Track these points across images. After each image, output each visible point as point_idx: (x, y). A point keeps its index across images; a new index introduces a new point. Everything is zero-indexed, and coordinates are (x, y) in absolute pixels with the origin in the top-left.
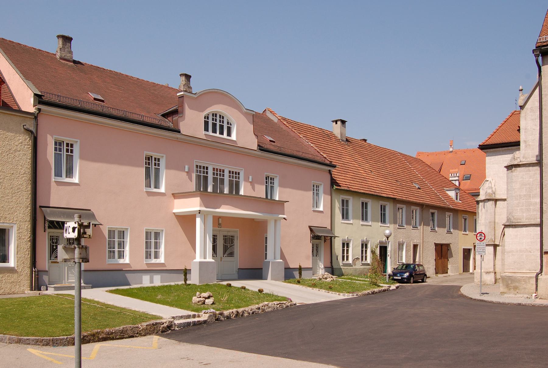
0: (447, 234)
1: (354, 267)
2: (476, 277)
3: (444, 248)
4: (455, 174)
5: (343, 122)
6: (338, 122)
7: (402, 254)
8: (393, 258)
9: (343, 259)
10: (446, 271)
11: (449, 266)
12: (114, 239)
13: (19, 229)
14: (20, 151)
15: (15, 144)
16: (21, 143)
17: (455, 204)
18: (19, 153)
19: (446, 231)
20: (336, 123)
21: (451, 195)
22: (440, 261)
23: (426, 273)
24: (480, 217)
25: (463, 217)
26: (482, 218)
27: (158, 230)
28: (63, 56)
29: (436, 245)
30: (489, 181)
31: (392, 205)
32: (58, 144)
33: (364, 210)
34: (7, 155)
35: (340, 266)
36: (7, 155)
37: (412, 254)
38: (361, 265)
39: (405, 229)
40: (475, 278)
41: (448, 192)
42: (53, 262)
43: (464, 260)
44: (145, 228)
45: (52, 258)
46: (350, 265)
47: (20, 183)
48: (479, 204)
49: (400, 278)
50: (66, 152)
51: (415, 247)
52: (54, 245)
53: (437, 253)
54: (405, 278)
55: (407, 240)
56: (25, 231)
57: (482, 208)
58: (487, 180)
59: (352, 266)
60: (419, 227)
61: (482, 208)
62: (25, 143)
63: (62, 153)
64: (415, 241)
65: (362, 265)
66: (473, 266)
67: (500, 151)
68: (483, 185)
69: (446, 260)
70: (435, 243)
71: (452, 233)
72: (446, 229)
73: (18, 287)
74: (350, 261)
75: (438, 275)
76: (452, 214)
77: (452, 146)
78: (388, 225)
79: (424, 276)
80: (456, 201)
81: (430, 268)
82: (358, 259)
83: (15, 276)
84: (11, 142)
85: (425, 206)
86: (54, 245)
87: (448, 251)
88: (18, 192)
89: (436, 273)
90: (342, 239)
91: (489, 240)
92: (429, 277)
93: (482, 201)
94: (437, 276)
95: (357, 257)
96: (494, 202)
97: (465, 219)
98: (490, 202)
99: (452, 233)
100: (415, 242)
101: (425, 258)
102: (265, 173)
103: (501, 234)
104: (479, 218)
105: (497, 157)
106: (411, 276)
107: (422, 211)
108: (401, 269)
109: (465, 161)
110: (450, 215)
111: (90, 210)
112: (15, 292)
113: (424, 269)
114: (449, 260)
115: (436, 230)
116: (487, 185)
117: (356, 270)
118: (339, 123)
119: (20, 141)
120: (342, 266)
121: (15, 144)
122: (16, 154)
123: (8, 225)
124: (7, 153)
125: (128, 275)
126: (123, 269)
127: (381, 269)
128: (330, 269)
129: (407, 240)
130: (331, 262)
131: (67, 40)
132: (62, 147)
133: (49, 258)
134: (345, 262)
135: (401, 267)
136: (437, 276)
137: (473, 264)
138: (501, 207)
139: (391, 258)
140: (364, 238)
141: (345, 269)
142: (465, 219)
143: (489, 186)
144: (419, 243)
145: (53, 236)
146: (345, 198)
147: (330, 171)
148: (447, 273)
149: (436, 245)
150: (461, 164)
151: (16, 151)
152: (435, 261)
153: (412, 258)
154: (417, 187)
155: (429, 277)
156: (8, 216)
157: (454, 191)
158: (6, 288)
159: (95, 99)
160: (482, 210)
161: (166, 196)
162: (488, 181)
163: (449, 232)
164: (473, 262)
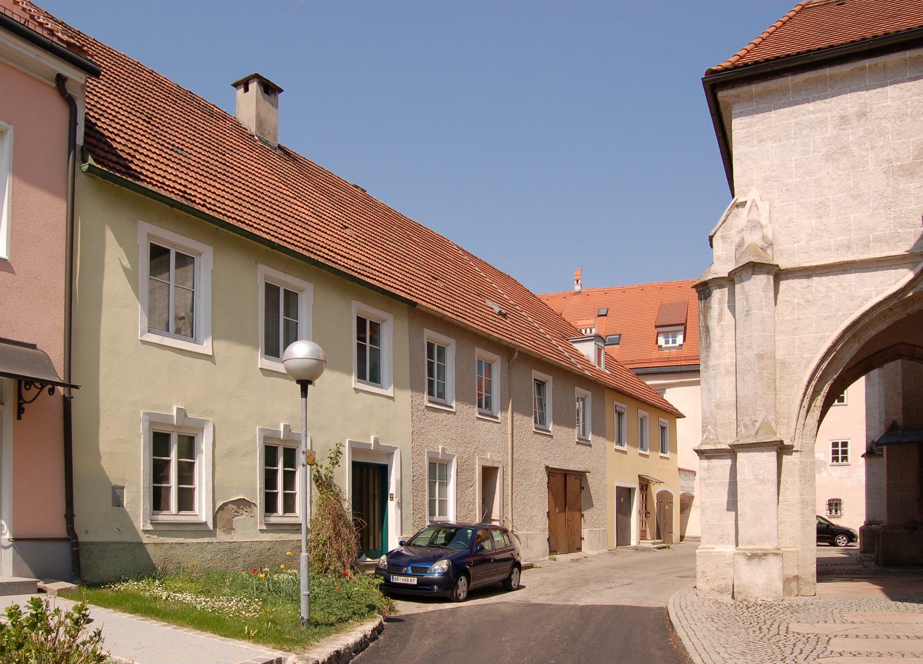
0: (579, 446)
1: (221, 537)
2: (703, 573)
3: (572, 482)
4: (588, 330)
5: (269, 89)
6: (250, 86)
7: (443, 493)
8: (408, 508)
9: (159, 501)
10: (577, 546)
11: (585, 532)
17: (596, 372)
19: (576, 436)
20: (246, 90)
21: (584, 354)
22: (561, 518)
23: (518, 559)
24: (715, 345)
25: (616, 406)
26: (721, 346)
29: (551, 472)
30: (748, 204)
31: (404, 326)
33: (282, 317)
35: (138, 535)
37: (477, 494)
38: (262, 531)
39: (454, 413)
40: (698, 576)
41: (576, 346)
43: (618, 514)
46: (198, 529)
48: (710, 295)
49: (415, 583)
51: (489, 474)
53: (553, 495)
54: (431, 583)
55: (461, 450)
57: (721, 311)
58: (741, 200)
59: (212, 533)
60: (499, 416)
61: (721, 311)
64: (489, 457)
65: (265, 528)
66: (637, 533)
67: (787, 90)
68: (725, 221)
69: (577, 514)
70: (547, 467)
71: (590, 446)
72: (576, 430)
74: (203, 510)
75: (558, 557)
76: (589, 393)
77: (579, 282)
78: (390, 392)
79: (513, 567)
80: (598, 367)
81: (534, 538)
82: (243, 504)
85: (516, 354)
87: (581, 491)
89: (552, 551)
90: (145, 413)
91: (757, 425)
92: (530, 567)
93: (719, 282)
94: (555, 559)
95: (242, 497)
96: (771, 278)
97: (620, 414)
98: (760, 276)
99: (590, 446)
100: (488, 460)
101: (519, 510)
103: (799, 403)
104: (712, 349)
105: (773, 114)
106: (458, 569)
107: (509, 368)
108: (431, 544)
109: (606, 310)
110: (586, 396)
113: (511, 542)
114: (583, 515)
115: (550, 432)
116: (741, 217)
117: (232, 549)
118: (254, 86)
120: (145, 531)
127: (348, 543)
128: (64, 550)
129: (461, 450)
130: (70, 517)
134: (172, 513)
135: (429, 534)
136: (555, 559)
137: (637, 527)
138: (796, 301)
139: (400, 505)
140: (278, 426)
141: (165, 546)
142: (620, 414)
143: (749, 221)
144: (499, 462)
146: (174, 245)
147: (61, 80)
148: (579, 549)
149: (551, 472)
150: (599, 316)
152: (548, 516)
153: (477, 508)
154: (497, 310)
155: (530, 567)
157: (593, 342)
160: (720, 315)
162: (743, 204)
163: (583, 442)
164: (637, 520)
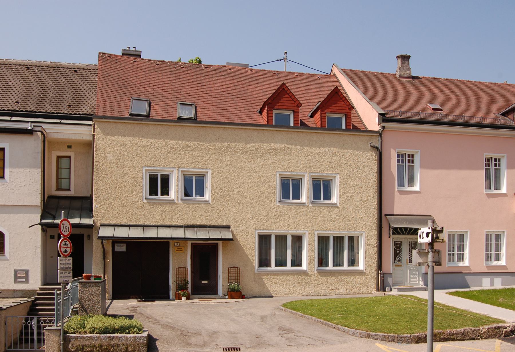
12: (454, 242)
13: (367, 236)
14: (367, 167)
15: (364, 161)
16: (369, 159)
18: (367, 168)
27: (489, 231)
28: (402, 74)
32: (401, 156)
34: (357, 171)
36: (357, 171)
42: (397, 265)
44: (485, 230)
45: (395, 262)
47: (368, 195)
50: (408, 163)
52: (398, 249)
56: (373, 238)
62: (372, 159)
63: (404, 164)
73: (366, 287)
83: (364, 278)
84: (360, 159)
86: (398, 249)
88: (366, 204)
102: (485, 154)
111: (430, 216)
112: (364, 292)
119: (368, 158)
121: (364, 161)
122: (365, 170)
123: (358, 233)
124: (357, 169)
125: (468, 278)
126: (463, 272)
131: (405, 58)
132: (404, 159)
133: (393, 262)
145: (396, 242)
151: (364, 167)
156: (358, 225)
158: (357, 288)
159: (434, 109)
161: (508, 196)
